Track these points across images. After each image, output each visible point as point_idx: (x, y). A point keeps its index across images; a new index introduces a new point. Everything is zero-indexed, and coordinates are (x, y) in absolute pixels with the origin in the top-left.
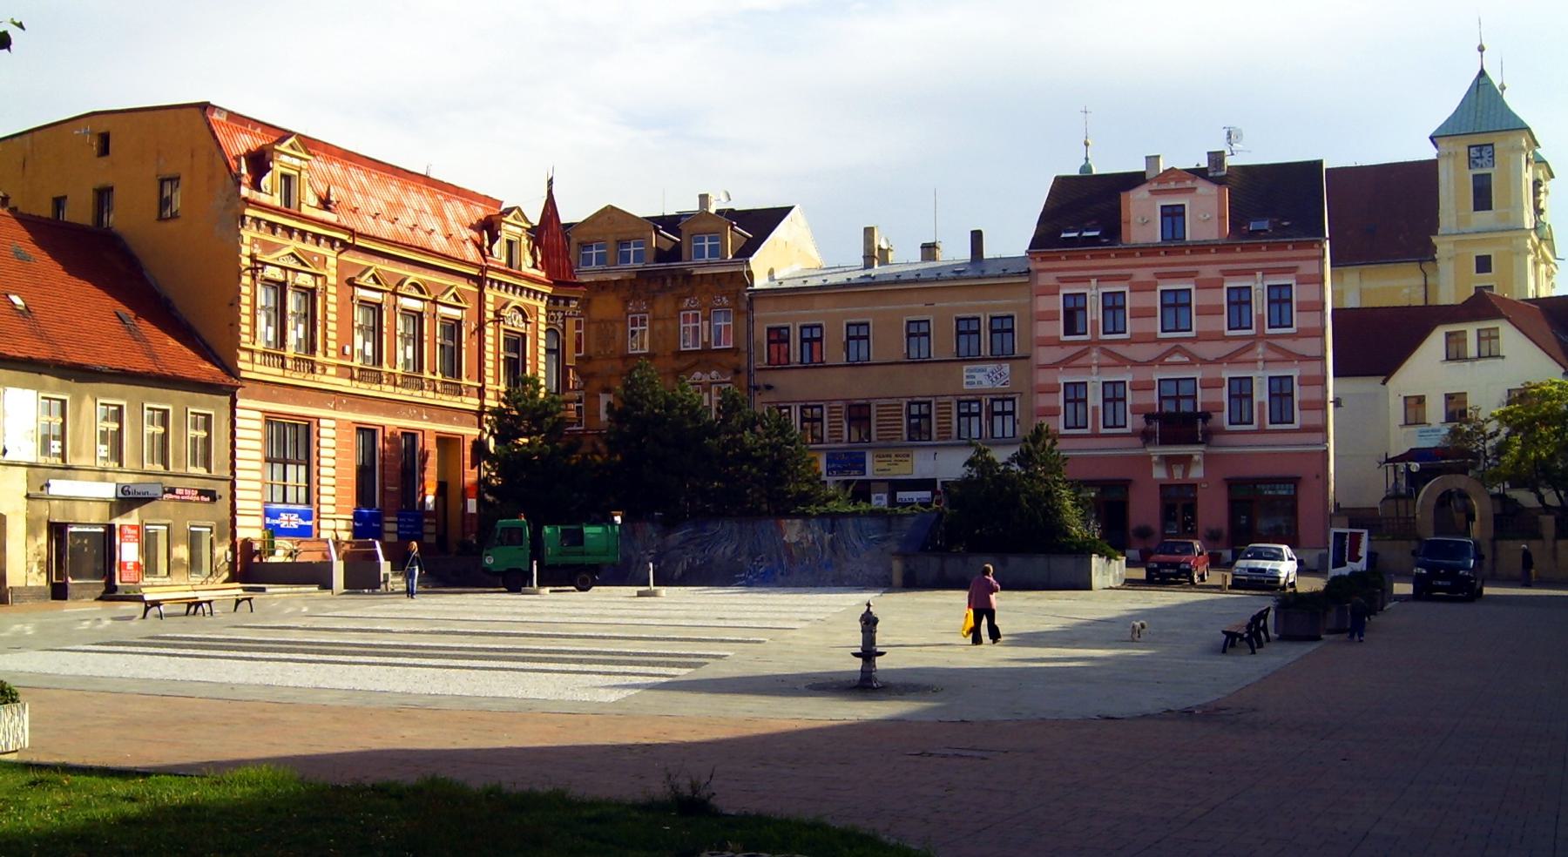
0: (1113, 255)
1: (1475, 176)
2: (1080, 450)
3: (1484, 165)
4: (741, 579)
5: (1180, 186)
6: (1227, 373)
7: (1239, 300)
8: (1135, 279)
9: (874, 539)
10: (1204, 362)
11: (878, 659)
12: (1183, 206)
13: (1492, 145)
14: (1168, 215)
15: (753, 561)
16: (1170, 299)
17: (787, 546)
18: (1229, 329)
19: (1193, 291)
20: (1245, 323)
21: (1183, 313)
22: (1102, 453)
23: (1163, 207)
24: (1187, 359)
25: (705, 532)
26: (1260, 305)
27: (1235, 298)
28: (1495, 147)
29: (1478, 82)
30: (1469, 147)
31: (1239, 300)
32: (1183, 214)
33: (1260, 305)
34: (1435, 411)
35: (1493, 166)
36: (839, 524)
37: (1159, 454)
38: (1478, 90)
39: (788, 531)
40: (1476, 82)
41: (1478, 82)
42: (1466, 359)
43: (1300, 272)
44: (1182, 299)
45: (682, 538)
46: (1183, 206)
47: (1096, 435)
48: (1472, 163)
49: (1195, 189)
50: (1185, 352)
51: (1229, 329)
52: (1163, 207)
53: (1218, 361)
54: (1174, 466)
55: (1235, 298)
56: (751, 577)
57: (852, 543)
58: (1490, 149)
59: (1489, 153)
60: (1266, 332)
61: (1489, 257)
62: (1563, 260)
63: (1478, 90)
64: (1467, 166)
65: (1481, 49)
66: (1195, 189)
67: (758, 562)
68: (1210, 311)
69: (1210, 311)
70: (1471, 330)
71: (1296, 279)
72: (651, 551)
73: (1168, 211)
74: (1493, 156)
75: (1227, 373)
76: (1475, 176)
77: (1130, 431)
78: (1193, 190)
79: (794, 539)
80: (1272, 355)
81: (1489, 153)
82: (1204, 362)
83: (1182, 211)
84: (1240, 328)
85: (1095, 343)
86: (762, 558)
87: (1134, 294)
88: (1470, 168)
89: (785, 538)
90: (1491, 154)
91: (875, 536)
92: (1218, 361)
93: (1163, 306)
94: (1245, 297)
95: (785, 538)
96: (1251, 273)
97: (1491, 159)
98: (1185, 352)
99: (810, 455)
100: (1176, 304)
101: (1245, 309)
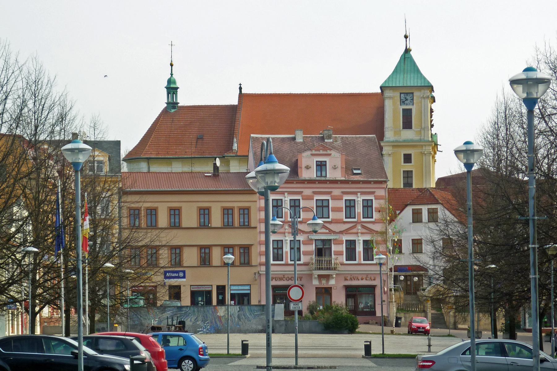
0: (295, 183)
1: (404, 110)
2: (289, 271)
3: (408, 104)
4: (201, 331)
5: (325, 153)
6: (345, 238)
7: (350, 206)
8: (304, 194)
9: (257, 314)
10: (334, 232)
11: (540, 356)
12: (326, 162)
13: (413, 93)
14: (416, 213)
15: (204, 323)
16: (320, 204)
17: (220, 317)
18: (346, 218)
19: (330, 201)
20: (353, 216)
21: (325, 209)
22: (289, 273)
23: (317, 161)
24: (327, 231)
25: (182, 311)
26: (359, 209)
27: (348, 204)
28: (414, 94)
29: (405, 56)
30: (401, 93)
31: (350, 206)
32: (326, 165)
33: (359, 209)
34: (407, 247)
35: (413, 105)
36: (242, 309)
37: (317, 274)
38: (404, 60)
39: (219, 311)
40: (403, 57)
41: (405, 56)
42: (421, 221)
43: (376, 194)
44: (325, 204)
45: (60, 325)
46: (326, 162)
47: (287, 265)
48: (402, 102)
49: (331, 154)
50: (327, 228)
51: (346, 218)
52: (317, 161)
53: (341, 232)
54: (322, 279)
55: (348, 204)
56: (204, 330)
57: (247, 316)
58: (411, 95)
59: (411, 97)
60: (362, 220)
61: (410, 155)
62: (442, 152)
63: (404, 60)
64: (400, 104)
65: (406, 37)
66: (331, 154)
67: (207, 324)
68: (337, 210)
69: (337, 210)
70: (425, 209)
71: (375, 196)
72: (156, 320)
73: (416, 211)
74: (413, 99)
75: (345, 238)
76: (404, 110)
77: (302, 263)
78: (330, 155)
79: (222, 314)
80: (364, 231)
81: (411, 97)
82: (334, 232)
83: (325, 163)
84: (350, 218)
85: (286, 222)
86: (208, 322)
87: (333, 212)
88: (401, 105)
89: (218, 314)
90: (412, 98)
91: (257, 313)
92: (341, 232)
93: (317, 206)
94: (352, 204)
95: (218, 314)
96: (355, 193)
97: (412, 101)
98: (327, 228)
99: (469, 318)
100: (323, 207)
101: (352, 209)
